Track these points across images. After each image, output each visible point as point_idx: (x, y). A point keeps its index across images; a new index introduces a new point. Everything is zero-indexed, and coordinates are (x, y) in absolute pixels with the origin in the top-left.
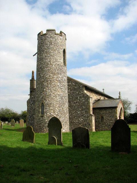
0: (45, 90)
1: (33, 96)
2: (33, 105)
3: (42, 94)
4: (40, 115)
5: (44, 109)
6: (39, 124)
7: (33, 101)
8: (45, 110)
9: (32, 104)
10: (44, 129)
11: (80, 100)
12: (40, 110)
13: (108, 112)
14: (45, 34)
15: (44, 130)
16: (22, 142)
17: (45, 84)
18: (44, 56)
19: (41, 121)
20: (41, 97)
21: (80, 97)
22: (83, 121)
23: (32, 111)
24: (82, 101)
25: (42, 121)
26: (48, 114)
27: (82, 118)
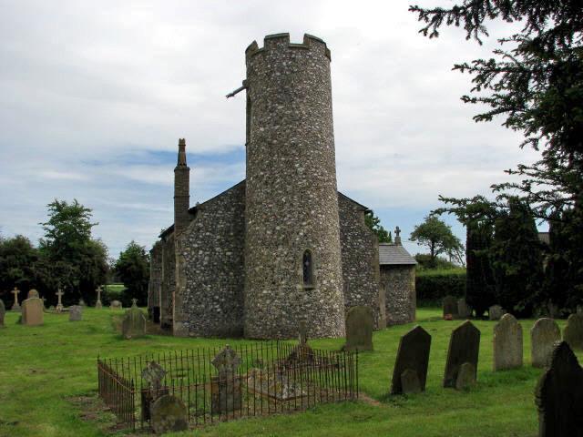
0: (313, 212)
1: (201, 225)
2: (201, 252)
3: (304, 223)
4: (299, 286)
5: (311, 270)
6: (298, 314)
7: (202, 240)
8: (316, 273)
9: (199, 248)
10: (316, 326)
11: (352, 245)
12: (301, 272)
13: (392, 276)
14: (263, 51)
15: (317, 330)
16: (443, 390)
17: (311, 196)
18: (304, 112)
19: (305, 304)
20: (301, 234)
21: (354, 237)
22: (360, 299)
23: (198, 272)
24: (358, 249)
25: (309, 303)
26: (325, 282)
27: (359, 293)
